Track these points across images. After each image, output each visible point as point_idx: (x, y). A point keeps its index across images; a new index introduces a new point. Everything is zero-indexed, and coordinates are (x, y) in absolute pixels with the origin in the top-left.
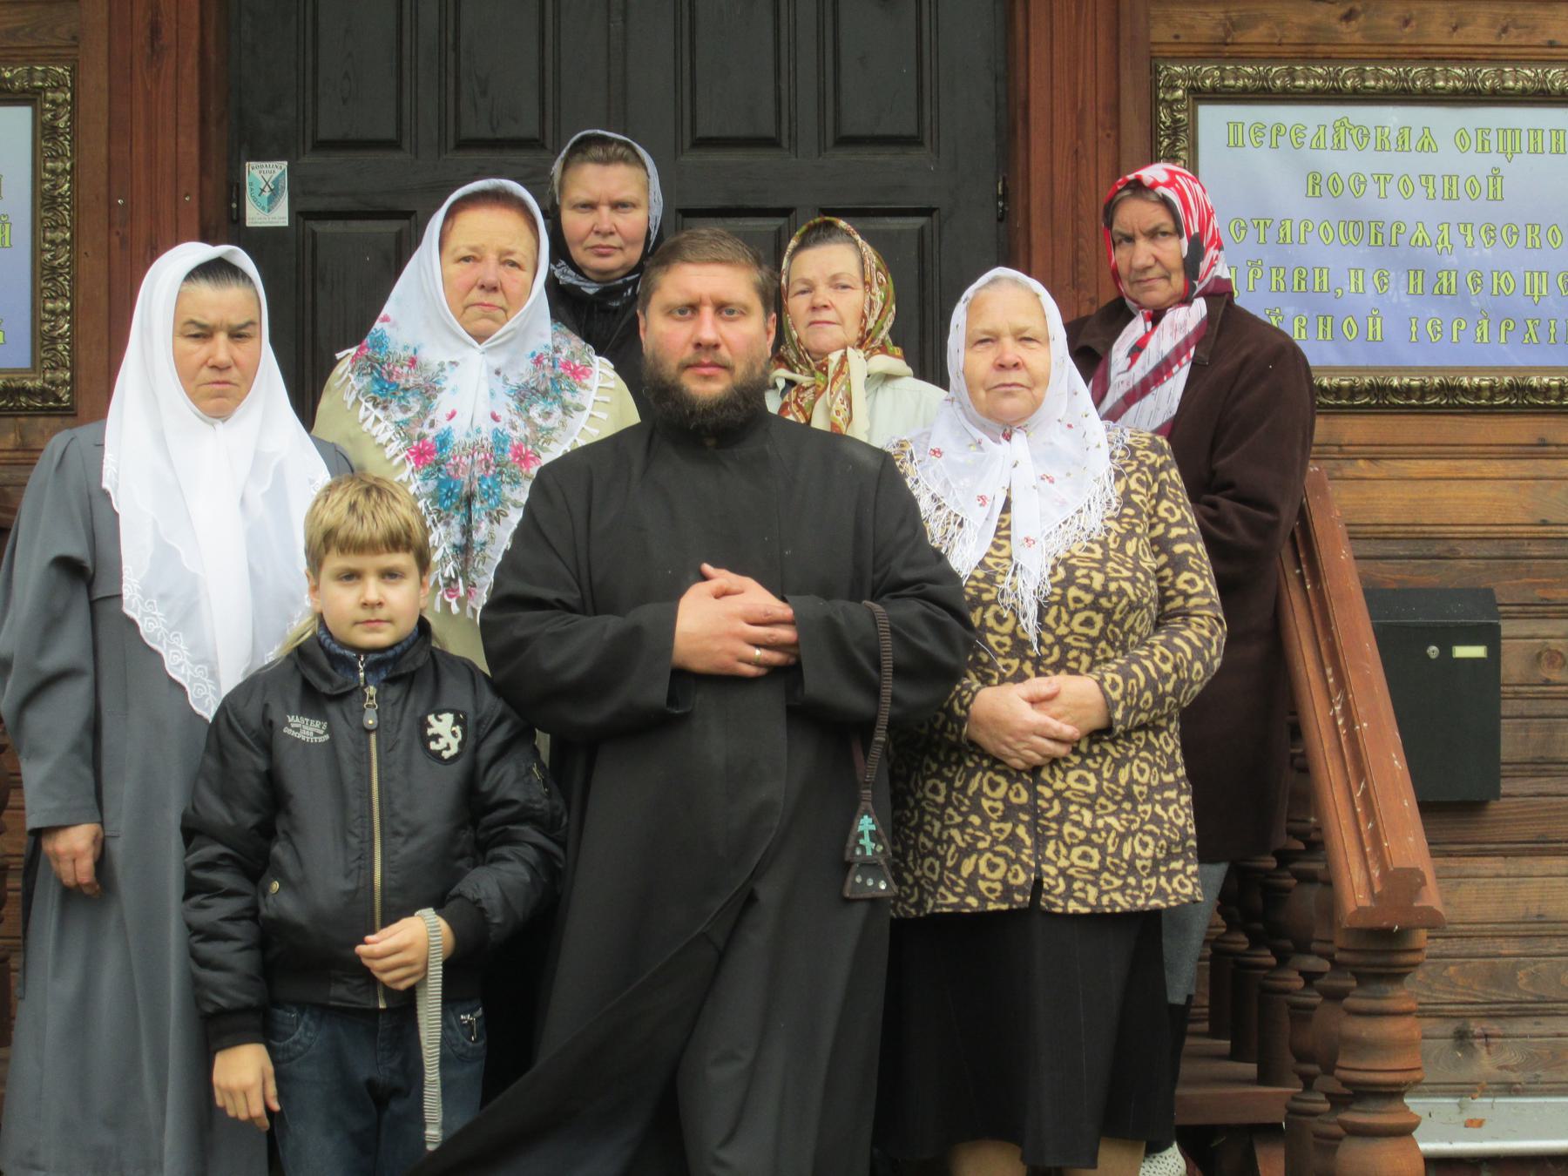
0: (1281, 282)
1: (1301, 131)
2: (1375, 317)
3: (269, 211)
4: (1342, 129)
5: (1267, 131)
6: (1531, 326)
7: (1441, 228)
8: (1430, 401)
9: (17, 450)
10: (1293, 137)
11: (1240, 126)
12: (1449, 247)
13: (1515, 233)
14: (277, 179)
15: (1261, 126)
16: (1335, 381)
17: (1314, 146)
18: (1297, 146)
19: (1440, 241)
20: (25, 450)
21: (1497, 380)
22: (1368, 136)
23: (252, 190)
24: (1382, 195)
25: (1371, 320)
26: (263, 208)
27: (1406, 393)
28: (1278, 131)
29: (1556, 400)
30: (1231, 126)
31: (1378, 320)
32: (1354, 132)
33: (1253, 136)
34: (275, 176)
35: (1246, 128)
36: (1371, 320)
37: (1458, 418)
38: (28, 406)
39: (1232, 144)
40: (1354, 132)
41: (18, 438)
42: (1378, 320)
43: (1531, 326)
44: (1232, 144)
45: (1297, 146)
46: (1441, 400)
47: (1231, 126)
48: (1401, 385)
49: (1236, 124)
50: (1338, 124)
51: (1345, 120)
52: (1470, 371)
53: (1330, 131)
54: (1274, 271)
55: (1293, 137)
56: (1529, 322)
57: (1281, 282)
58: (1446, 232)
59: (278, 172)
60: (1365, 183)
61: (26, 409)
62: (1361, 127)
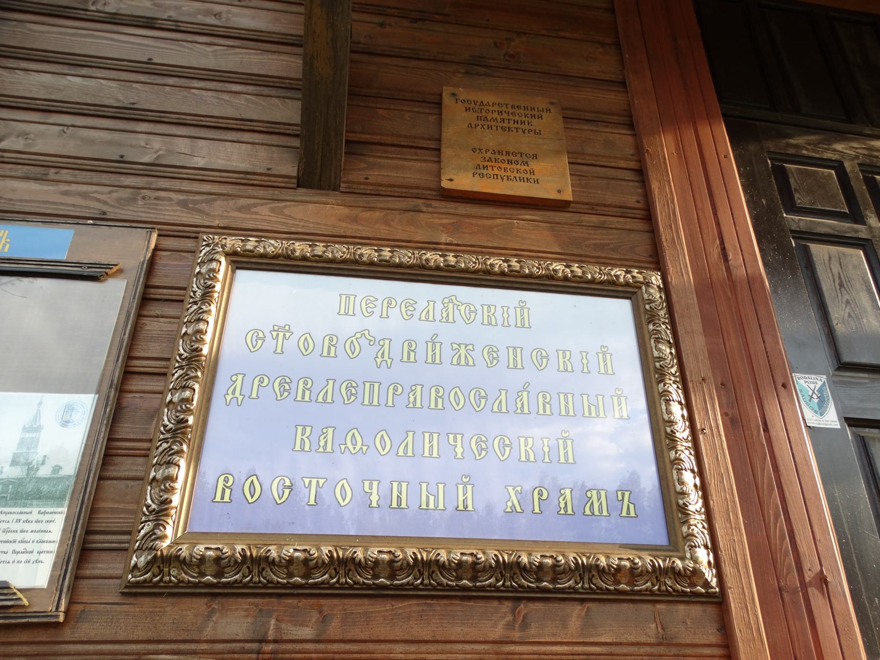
0: (307, 441)
1: (411, 305)
2: (465, 485)
3: (822, 415)
4: (451, 305)
5: (379, 303)
6: (512, 493)
7: (234, 378)
8: (644, 585)
9: (659, 644)
10: (364, 307)
11: (352, 298)
12: (240, 398)
13: (483, 397)
14: (820, 390)
15: (412, 302)
16: (456, 556)
17: (423, 317)
18: (406, 317)
19: (230, 392)
20: (669, 645)
21: (398, 553)
22: (475, 312)
23: (803, 396)
24: (279, 351)
25: (461, 487)
26: (816, 412)
27: (198, 566)
28: (389, 304)
29: (214, 576)
30: (344, 297)
31: (469, 487)
32: (462, 308)
33: (364, 307)
34: (818, 387)
35: (358, 300)
36: (461, 487)
37: (556, 605)
38: (180, 581)
39: (342, 312)
40: (462, 308)
41: (661, 631)
42: (469, 487)
43: (512, 493)
44: (342, 312)
45: (406, 317)
46: (498, 581)
47: (344, 297)
48: (191, 556)
49: (348, 296)
50: (446, 301)
51: (453, 298)
52: (281, 539)
53: (439, 306)
54: (300, 429)
55: (403, 310)
56: (510, 489)
57: (307, 441)
58: (239, 383)
59: (820, 384)
60: (263, 339)
61: (176, 586)
62: (468, 304)
